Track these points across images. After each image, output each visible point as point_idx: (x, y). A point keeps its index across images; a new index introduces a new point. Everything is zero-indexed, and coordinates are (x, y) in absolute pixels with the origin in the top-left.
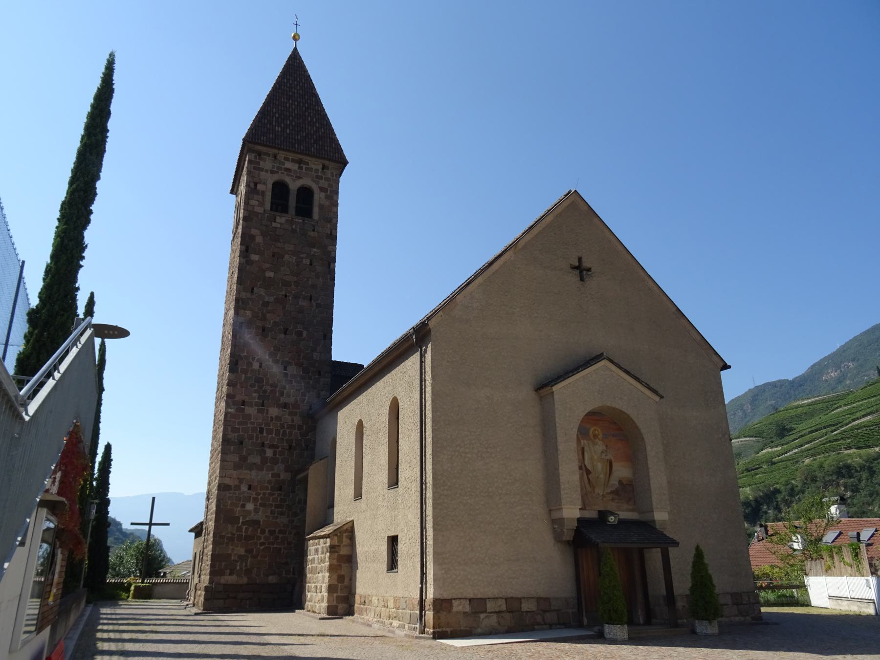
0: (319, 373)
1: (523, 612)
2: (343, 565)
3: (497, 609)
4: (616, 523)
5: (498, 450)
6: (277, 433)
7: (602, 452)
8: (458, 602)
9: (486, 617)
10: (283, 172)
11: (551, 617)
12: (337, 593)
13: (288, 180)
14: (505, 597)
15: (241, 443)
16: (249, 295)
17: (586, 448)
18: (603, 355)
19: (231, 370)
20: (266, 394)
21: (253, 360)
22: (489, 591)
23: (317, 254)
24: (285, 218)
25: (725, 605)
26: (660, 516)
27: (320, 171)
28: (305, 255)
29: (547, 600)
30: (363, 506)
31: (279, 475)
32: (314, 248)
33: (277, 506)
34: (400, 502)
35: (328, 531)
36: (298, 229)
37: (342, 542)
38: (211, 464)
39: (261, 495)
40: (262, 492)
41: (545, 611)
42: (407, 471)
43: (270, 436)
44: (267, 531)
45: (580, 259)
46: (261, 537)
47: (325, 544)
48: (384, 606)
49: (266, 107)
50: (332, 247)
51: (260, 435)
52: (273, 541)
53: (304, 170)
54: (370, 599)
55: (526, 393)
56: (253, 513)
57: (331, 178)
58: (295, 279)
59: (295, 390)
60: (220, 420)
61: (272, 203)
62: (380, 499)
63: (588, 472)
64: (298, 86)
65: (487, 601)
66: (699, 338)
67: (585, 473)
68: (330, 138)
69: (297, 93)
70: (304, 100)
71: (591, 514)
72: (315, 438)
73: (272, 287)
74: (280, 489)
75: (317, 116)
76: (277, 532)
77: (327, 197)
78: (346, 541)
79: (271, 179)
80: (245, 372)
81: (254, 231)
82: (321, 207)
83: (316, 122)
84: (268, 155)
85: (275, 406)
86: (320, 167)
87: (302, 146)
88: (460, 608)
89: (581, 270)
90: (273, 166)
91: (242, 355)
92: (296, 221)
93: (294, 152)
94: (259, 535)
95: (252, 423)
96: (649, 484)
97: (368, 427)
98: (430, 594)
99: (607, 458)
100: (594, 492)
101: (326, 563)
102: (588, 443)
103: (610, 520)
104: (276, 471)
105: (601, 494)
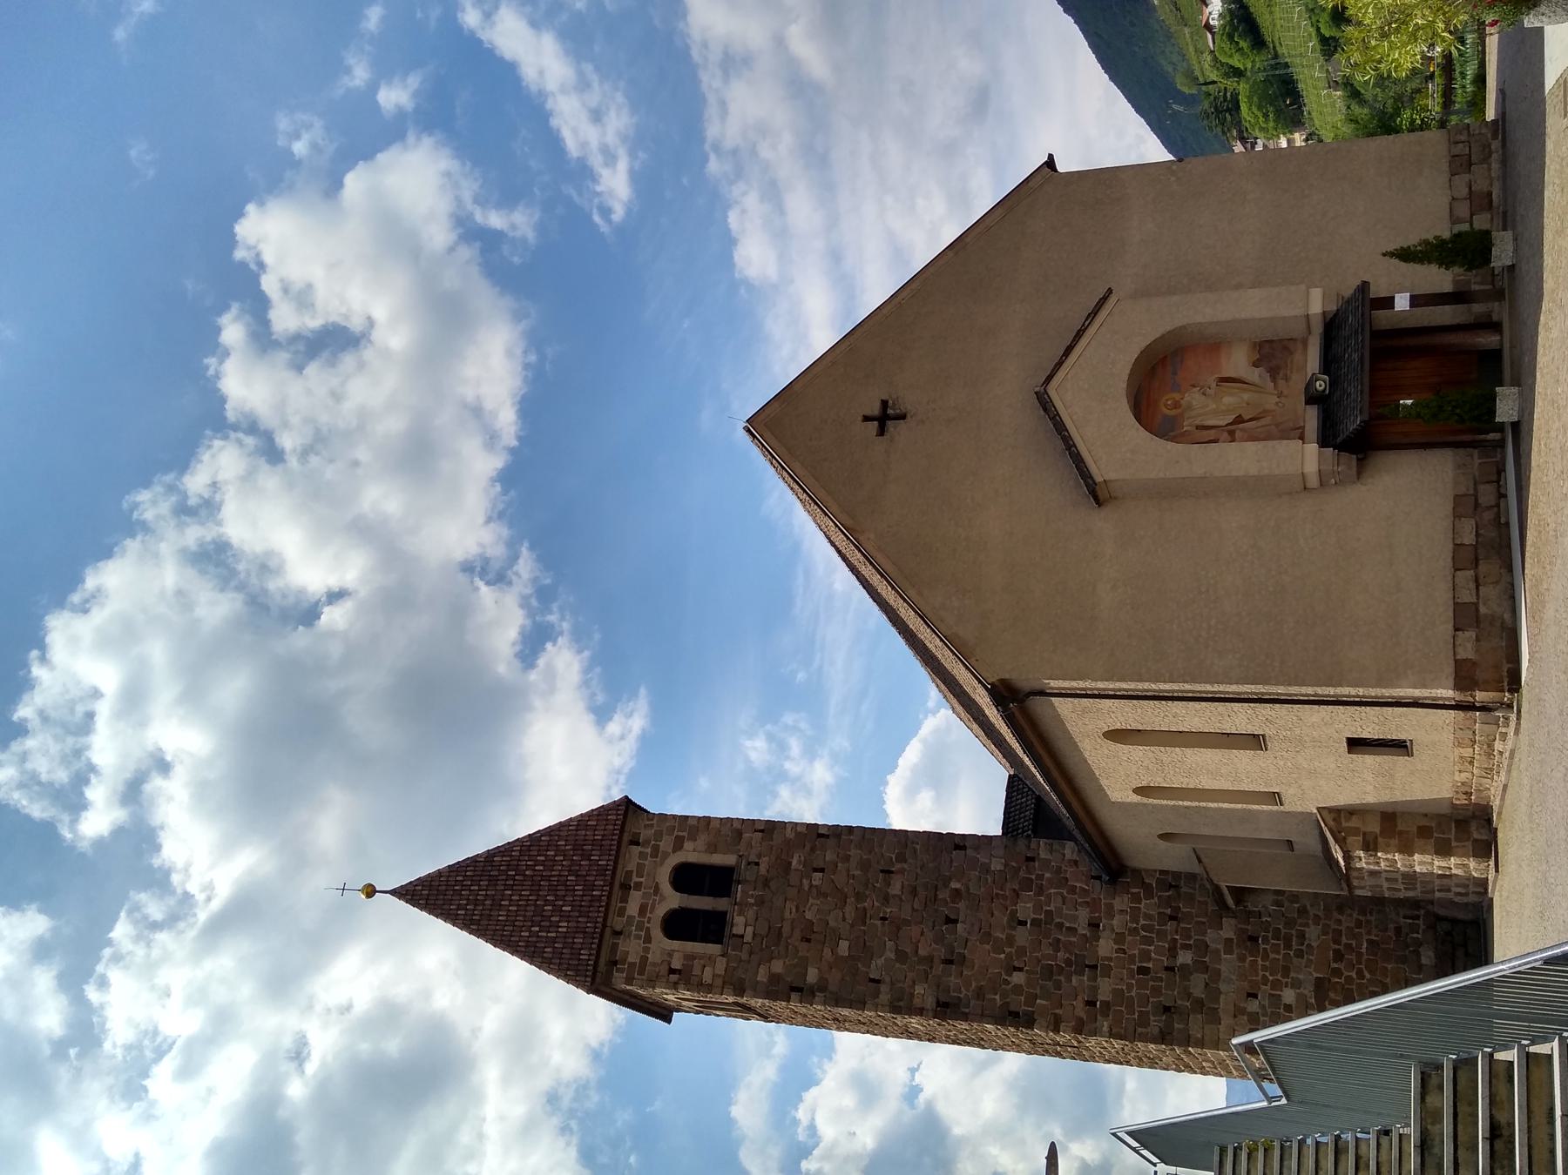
0: (1030, 859)
1: (1477, 542)
2: (1400, 828)
3: (1472, 585)
4: (1326, 377)
5: (1203, 573)
6: (1148, 941)
7: (1204, 394)
8: (1460, 650)
9: (1484, 604)
10: (646, 920)
11: (1487, 495)
12: (1450, 839)
13: (661, 911)
14: (1453, 570)
15: (1167, 1009)
16: (884, 988)
17: (1198, 422)
18: (1039, 392)
19: (1028, 1021)
20: (1073, 959)
21: (1009, 983)
22: (1443, 595)
23: (802, 858)
24: (735, 917)
25: (1470, 188)
26: (1317, 304)
27: (642, 850)
28: (804, 881)
29: (1458, 499)
30: (1291, 791)
31: (1228, 941)
32: (790, 863)
33: (1288, 946)
34: (1289, 733)
35: (1336, 852)
36: (756, 893)
37: (1357, 829)
38: (1204, 1072)
39: (1267, 974)
40: (1261, 973)
41: (1477, 505)
42: (1236, 720)
43: (1153, 955)
44: (1335, 965)
45: (866, 419)
46: (1347, 977)
47: (1361, 860)
48: (1471, 763)
49: (519, 949)
50: (789, 830)
51: (1152, 974)
52: (1354, 954)
53: (641, 880)
54: (1459, 784)
55: (1103, 522)
56: (1302, 990)
57: (655, 828)
58: (852, 900)
59: (1064, 907)
60: (1123, 1049)
61: (705, 940)
62: (1282, 763)
63: (1239, 420)
64: (472, 888)
65: (1459, 601)
66: (1000, 211)
67: (1241, 426)
68: (577, 830)
69: (486, 890)
70: (500, 878)
71: (1311, 418)
72: (1155, 871)
73: (868, 944)
74: (1253, 939)
75: (531, 853)
76: (1337, 947)
77: (693, 838)
78: (1354, 822)
79: (662, 944)
80: (1032, 999)
81: (762, 976)
82: (712, 848)
83: (546, 856)
84: (615, 947)
85: (1094, 943)
86: (636, 850)
87: (596, 883)
88: (1469, 646)
89: (885, 418)
90: (638, 937)
91: (999, 1003)
92: (741, 897)
93: (609, 897)
94: (1343, 980)
95: (1130, 987)
96: (1261, 319)
97: (1150, 779)
98: (1447, 693)
99: (1214, 385)
100: (1274, 411)
101: (1396, 858)
102: (1188, 418)
103: (1322, 388)
104: (1221, 947)
105: (1278, 400)
